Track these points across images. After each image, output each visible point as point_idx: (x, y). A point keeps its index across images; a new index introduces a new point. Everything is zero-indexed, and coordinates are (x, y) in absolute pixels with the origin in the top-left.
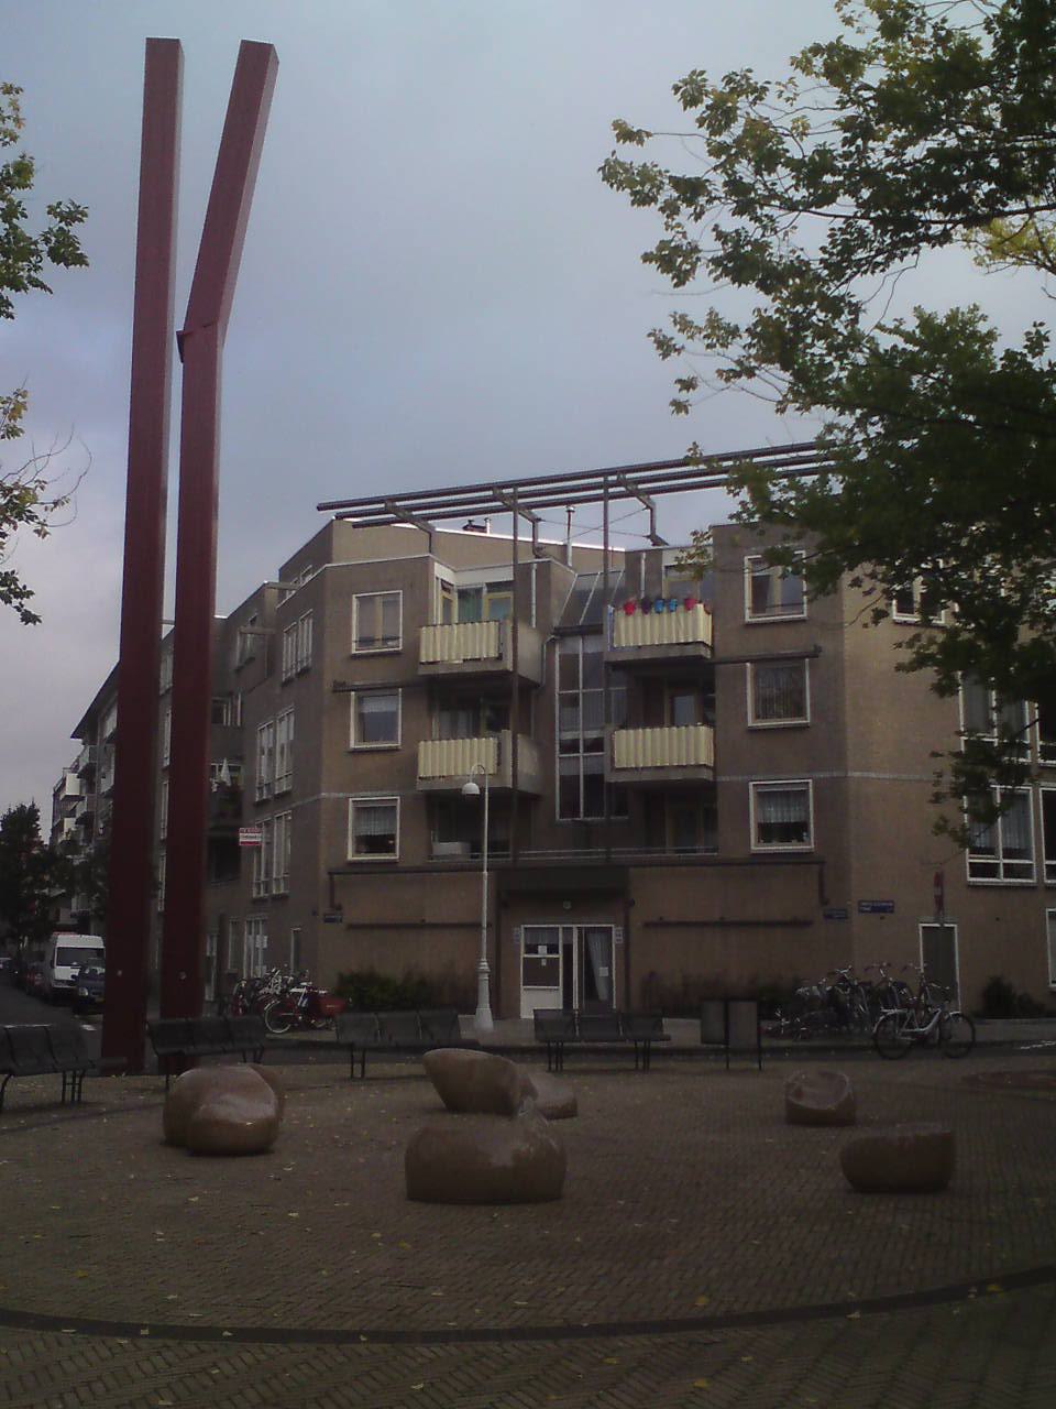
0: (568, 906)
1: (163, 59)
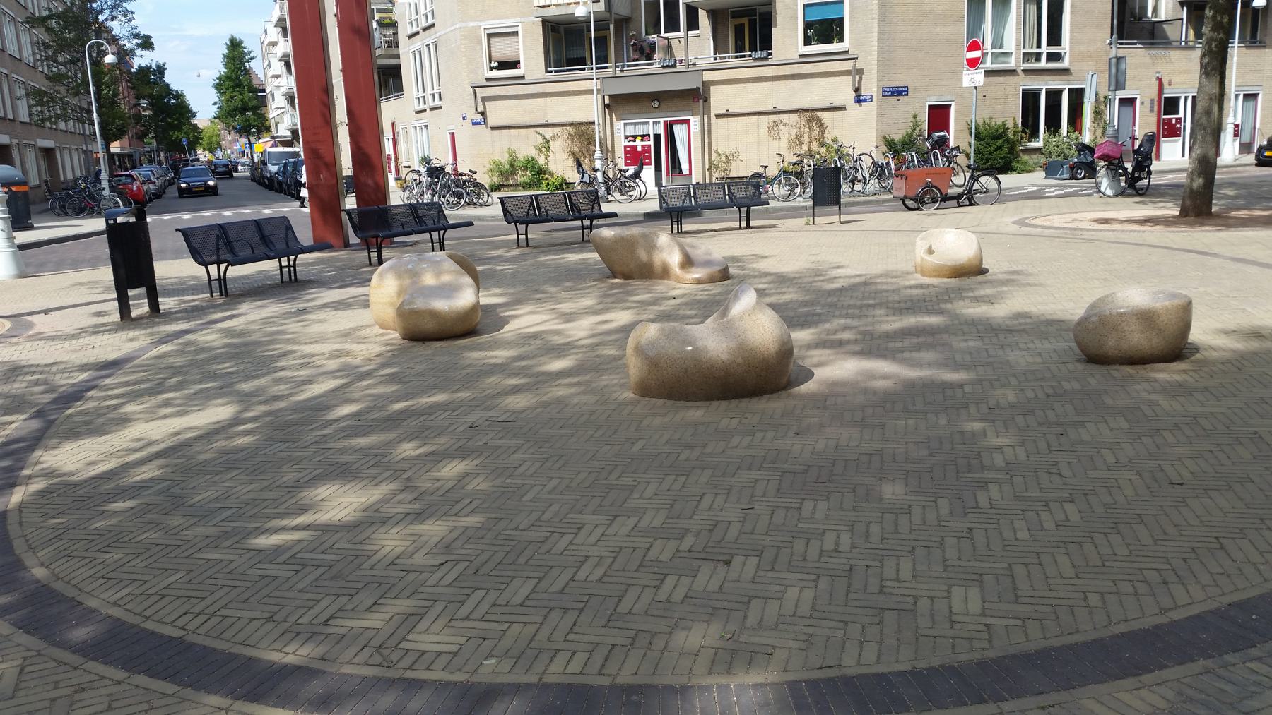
0: (656, 104)
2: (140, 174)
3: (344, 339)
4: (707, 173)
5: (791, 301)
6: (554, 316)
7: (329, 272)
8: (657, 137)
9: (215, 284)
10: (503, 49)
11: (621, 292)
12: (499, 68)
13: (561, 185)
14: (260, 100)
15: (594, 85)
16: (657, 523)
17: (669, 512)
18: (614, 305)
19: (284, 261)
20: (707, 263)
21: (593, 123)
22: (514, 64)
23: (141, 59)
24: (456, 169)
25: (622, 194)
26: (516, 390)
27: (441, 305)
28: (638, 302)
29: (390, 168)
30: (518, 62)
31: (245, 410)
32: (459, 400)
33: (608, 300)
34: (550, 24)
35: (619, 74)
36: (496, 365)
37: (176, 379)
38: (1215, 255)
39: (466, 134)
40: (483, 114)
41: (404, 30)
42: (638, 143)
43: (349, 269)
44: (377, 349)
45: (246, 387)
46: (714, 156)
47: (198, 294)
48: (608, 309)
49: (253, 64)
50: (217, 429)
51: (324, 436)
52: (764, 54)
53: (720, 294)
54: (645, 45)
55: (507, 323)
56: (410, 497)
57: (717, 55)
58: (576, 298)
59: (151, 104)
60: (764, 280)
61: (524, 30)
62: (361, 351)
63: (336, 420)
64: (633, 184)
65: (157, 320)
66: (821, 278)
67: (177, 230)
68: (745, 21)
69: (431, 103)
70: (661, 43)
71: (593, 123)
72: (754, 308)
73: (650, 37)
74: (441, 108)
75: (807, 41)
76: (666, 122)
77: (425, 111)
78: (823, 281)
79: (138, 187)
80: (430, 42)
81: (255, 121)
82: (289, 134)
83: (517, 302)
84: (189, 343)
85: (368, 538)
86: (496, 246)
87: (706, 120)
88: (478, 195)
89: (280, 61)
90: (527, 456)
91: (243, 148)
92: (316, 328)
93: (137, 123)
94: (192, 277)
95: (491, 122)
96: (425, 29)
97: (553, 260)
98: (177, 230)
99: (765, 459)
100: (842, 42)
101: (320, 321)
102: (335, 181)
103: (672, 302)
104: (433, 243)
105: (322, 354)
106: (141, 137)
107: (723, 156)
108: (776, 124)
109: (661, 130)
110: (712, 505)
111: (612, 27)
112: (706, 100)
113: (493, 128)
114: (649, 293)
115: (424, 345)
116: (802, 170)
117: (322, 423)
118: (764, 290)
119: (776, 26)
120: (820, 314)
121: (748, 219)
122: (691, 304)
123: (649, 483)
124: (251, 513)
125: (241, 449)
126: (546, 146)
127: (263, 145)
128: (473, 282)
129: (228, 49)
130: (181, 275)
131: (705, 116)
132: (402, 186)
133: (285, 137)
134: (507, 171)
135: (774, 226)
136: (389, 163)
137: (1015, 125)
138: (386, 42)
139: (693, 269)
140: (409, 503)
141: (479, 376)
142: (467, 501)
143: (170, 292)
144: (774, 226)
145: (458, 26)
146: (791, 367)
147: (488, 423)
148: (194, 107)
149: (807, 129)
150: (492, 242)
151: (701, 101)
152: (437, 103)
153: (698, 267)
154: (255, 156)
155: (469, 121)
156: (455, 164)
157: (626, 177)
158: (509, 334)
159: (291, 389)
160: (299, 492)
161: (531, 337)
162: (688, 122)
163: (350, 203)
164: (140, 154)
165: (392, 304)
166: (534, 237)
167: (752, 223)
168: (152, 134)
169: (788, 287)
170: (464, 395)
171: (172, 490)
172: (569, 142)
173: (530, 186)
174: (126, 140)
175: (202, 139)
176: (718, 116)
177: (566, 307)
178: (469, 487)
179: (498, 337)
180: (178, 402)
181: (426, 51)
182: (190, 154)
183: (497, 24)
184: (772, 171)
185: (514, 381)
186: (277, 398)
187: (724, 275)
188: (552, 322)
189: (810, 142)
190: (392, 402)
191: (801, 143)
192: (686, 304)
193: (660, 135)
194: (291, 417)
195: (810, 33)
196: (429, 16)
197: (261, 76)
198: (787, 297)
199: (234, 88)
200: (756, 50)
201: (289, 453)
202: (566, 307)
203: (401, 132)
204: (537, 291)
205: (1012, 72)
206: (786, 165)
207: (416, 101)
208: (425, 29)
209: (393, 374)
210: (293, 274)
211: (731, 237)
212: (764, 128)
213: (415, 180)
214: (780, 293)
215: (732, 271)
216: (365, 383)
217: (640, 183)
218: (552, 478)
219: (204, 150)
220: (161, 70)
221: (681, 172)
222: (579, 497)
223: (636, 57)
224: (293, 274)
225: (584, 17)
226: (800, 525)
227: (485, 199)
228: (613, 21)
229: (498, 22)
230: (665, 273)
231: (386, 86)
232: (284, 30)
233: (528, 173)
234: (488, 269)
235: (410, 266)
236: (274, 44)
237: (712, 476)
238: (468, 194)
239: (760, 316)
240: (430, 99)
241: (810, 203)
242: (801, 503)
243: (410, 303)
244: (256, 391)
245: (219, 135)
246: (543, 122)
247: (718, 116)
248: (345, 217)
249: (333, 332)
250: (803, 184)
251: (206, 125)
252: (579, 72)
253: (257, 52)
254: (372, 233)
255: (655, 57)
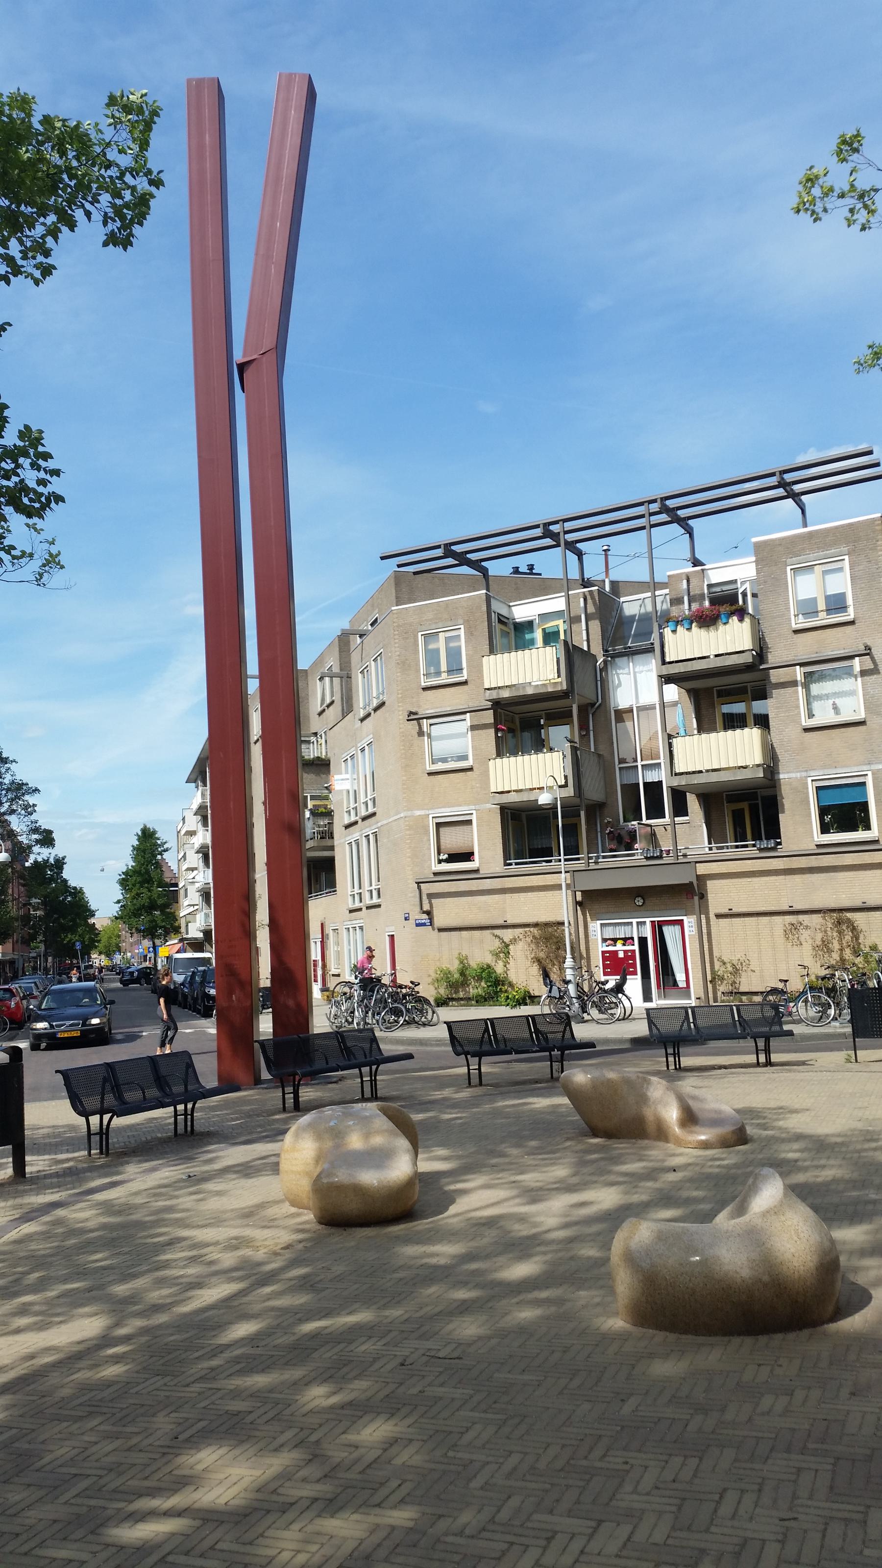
0: (639, 901)
1: (870, 453)
2: (20, 987)
3: (245, 1221)
4: (710, 986)
5: (835, 1181)
6: (514, 1192)
7: (233, 1120)
8: (643, 941)
9: (95, 1139)
10: (453, 840)
11: (602, 1159)
12: (447, 861)
13: (524, 999)
14: (171, 896)
15: (563, 879)
16: (659, 1536)
17: (676, 1518)
18: (594, 1178)
19: (181, 1107)
20: (716, 1121)
21: (563, 924)
22: (467, 856)
23: (40, 854)
24: (394, 981)
25: (600, 1011)
26: (464, 1308)
27: (369, 1178)
28: (626, 1174)
29: (315, 976)
30: (472, 854)
31: (117, 1325)
32: (389, 1320)
33: (585, 1170)
34: (509, 811)
35: (592, 866)
36: (436, 1267)
37: (36, 1275)
39: (406, 935)
40: (429, 913)
41: (341, 819)
43: (258, 1115)
44: (285, 1237)
45: (121, 1289)
46: (717, 965)
47: (74, 1152)
48: (585, 1184)
49: (166, 855)
50: (80, 1352)
51: (212, 1369)
52: (772, 844)
53: (736, 1166)
54: (623, 833)
55: (453, 1202)
56: (319, 1474)
57: (713, 845)
58: (546, 1165)
59: (44, 903)
60: (796, 1146)
61: (477, 819)
62: (266, 1239)
63: (228, 1346)
64: (614, 1000)
65: (21, 1188)
66: (873, 1145)
67: (57, 1072)
68: (745, 805)
69: (368, 901)
70: (643, 831)
71: (563, 924)
72: (781, 1203)
73: (629, 824)
74: (379, 906)
75: (825, 829)
76: (652, 922)
77: (360, 909)
78: (875, 1149)
79: (17, 1004)
80: (370, 833)
81: (163, 921)
82: (201, 935)
83: (467, 1169)
84: (59, 1222)
85: (262, 1535)
86: (442, 1083)
87: (704, 921)
88: (421, 1011)
89: (197, 852)
90: (477, 1414)
91: (146, 952)
92: (214, 1204)
93: (24, 926)
94: (68, 1126)
95: (439, 921)
96: (364, 819)
97: (513, 1106)
98: (57, 1072)
99: (809, 1436)
100: (870, 829)
101: (219, 1193)
102: (248, 1004)
103: (672, 1177)
104: (362, 1078)
105: (217, 1243)
106: (27, 941)
107: (728, 965)
108: (794, 927)
109: (648, 933)
110: (736, 1510)
111: (582, 813)
112: (703, 896)
113: (440, 930)
114: (640, 1160)
115: (345, 1233)
116: (834, 986)
117: (209, 1349)
118: (796, 1161)
119: (783, 812)
120: (874, 1202)
121: (767, 1051)
122: (701, 1179)
123: (646, 1467)
124: (112, 1486)
125: (108, 1384)
126: (505, 951)
127: (169, 949)
128: (410, 1146)
129: (138, 840)
130: (55, 1123)
131: (703, 916)
132: (329, 1000)
133: (196, 939)
134: (457, 981)
135: (803, 1063)
136: (315, 971)
138: (319, 832)
139: (697, 1128)
140: (318, 1481)
141: (414, 1284)
142: (394, 1483)
143: (42, 1148)
144: (803, 1063)
145: (402, 815)
146: (839, 1284)
147: (425, 1359)
148: (93, 906)
149: (835, 934)
150: (435, 1077)
151: (696, 898)
152: (375, 901)
153: (703, 1125)
154: (159, 961)
155: (412, 922)
156: (394, 974)
157: (605, 991)
158: (455, 1220)
159: (176, 1295)
160: (177, 1455)
161: (484, 1224)
162: (680, 923)
163: (265, 1025)
164: (24, 960)
165: (307, 1174)
166: (489, 1070)
167: (775, 1057)
168: (41, 938)
169: (828, 1158)
170: (395, 1313)
171: (16, 1445)
172: (533, 946)
173: (486, 1000)
174: (9, 945)
175: (99, 941)
176: (719, 916)
177: (530, 1178)
178: (398, 1461)
179: (441, 1223)
180: (37, 1308)
181: (364, 842)
182: (83, 959)
183: (447, 812)
184: (796, 985)
185: (462, 1294)
186: (157, 1308)
187: (740, 1137)
188: (511, 1203)
189: (841, 950)
190: (301, 1321)
191: (830, 951)
192: (691, 1180)
193: (646, 938)
194: (172, 1338)
195: (827, 819)
196: (370, 804)
197: (173, 865)
198: (827, 1174)
199: (142, 884)
200: (761, 839)
201: (167, 1394)
202: (530, 1178)
203: (331, 934)
204: (492, 1153)
206: (813, 978)
207: (350, 899)
208: (364, 819)
209: (304, 1277)
210: (189, 1123)
211: (746, 1077)
212: (779, 932)
213: (345, 994)
214: (817, 1167)
215: (749, 1130)
216: (268, 1290)
217: (624, 999)
218: (511, 1452)
219: (100, 953)
220: (59, 864)
221: (675, 984)
222: (548, 1486)
223: (613, 847)
224: (189, 1123)
225: (549, 804)
226: (867, 1552)
227: (429, 1017)
228: (584, 808)
229: (449, 810)
230: (661, 1133)
231: (318, 880)
232: (204, 819)
233: (483, 984)
234: (431, 1117)
235: (332, 1124)
236: (192, 833)
237: (736, 1460)
238: (408, 1010)
239: (789, 1214)
240: (366, 896)
241: (849, 1029)
242: (866, 1514)
243: (329, 1175)
244: (132, 1297)
245: (119, 936)
246: (500, 922)
247: (719, 916)
248: (256, 1045)
249: (232, 1210)
250: (837, 1004)
251: (105, 925)
252: (544, 864)
253: (171, 843)
254: (291, 1070)
255: (636, 846)
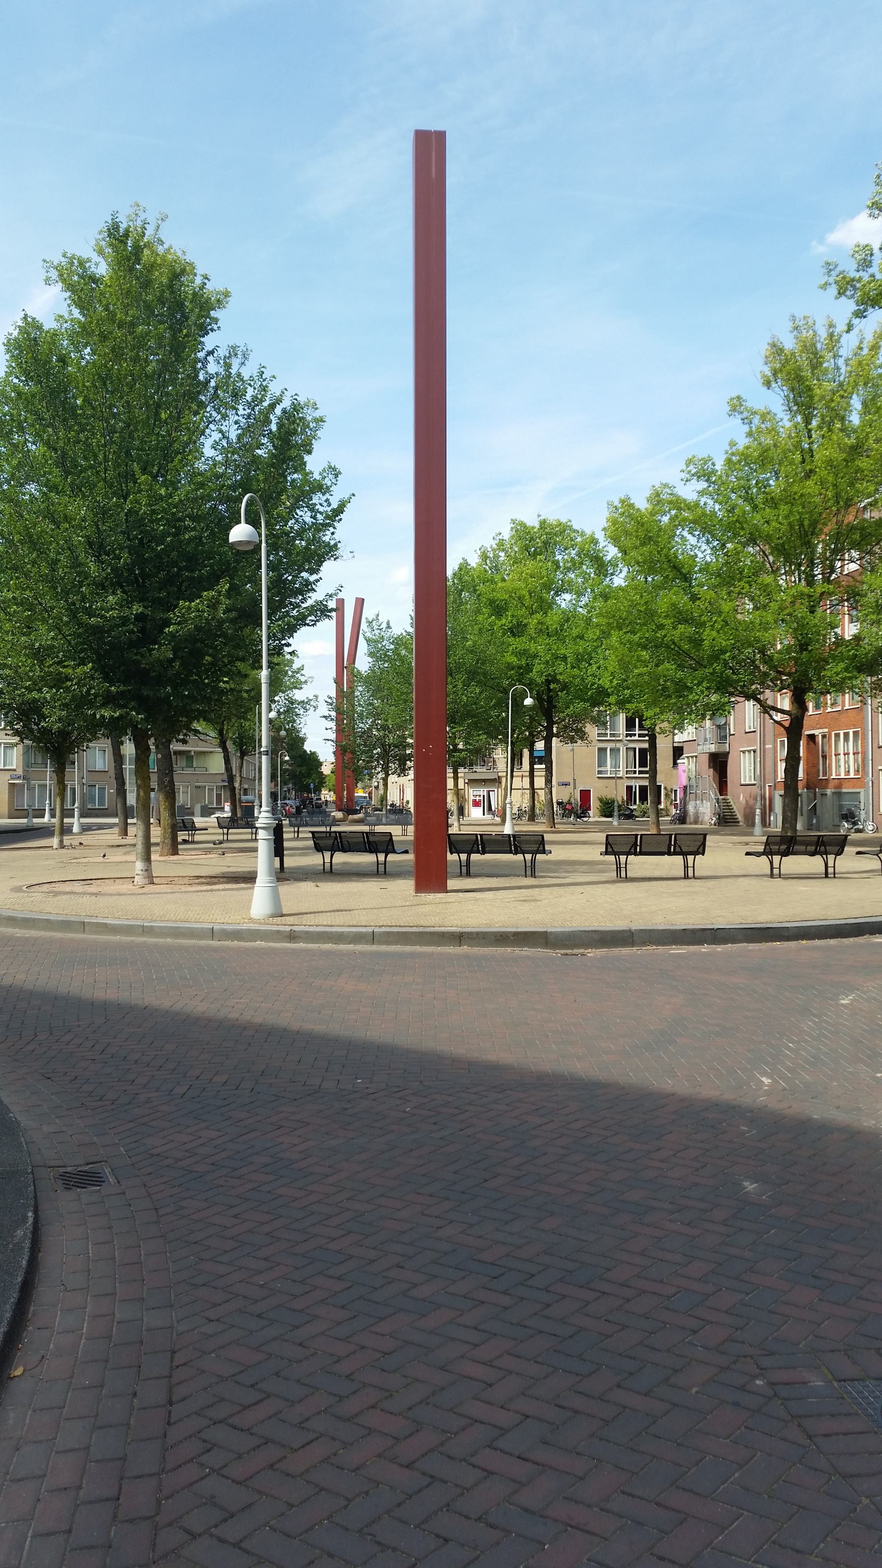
8: (484, 796)
38: (522, 901)
42: (477, 798)
137: (623, 799)
205: (621, 778)
219: (330, 791)
